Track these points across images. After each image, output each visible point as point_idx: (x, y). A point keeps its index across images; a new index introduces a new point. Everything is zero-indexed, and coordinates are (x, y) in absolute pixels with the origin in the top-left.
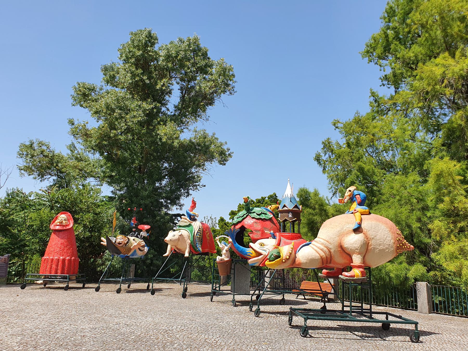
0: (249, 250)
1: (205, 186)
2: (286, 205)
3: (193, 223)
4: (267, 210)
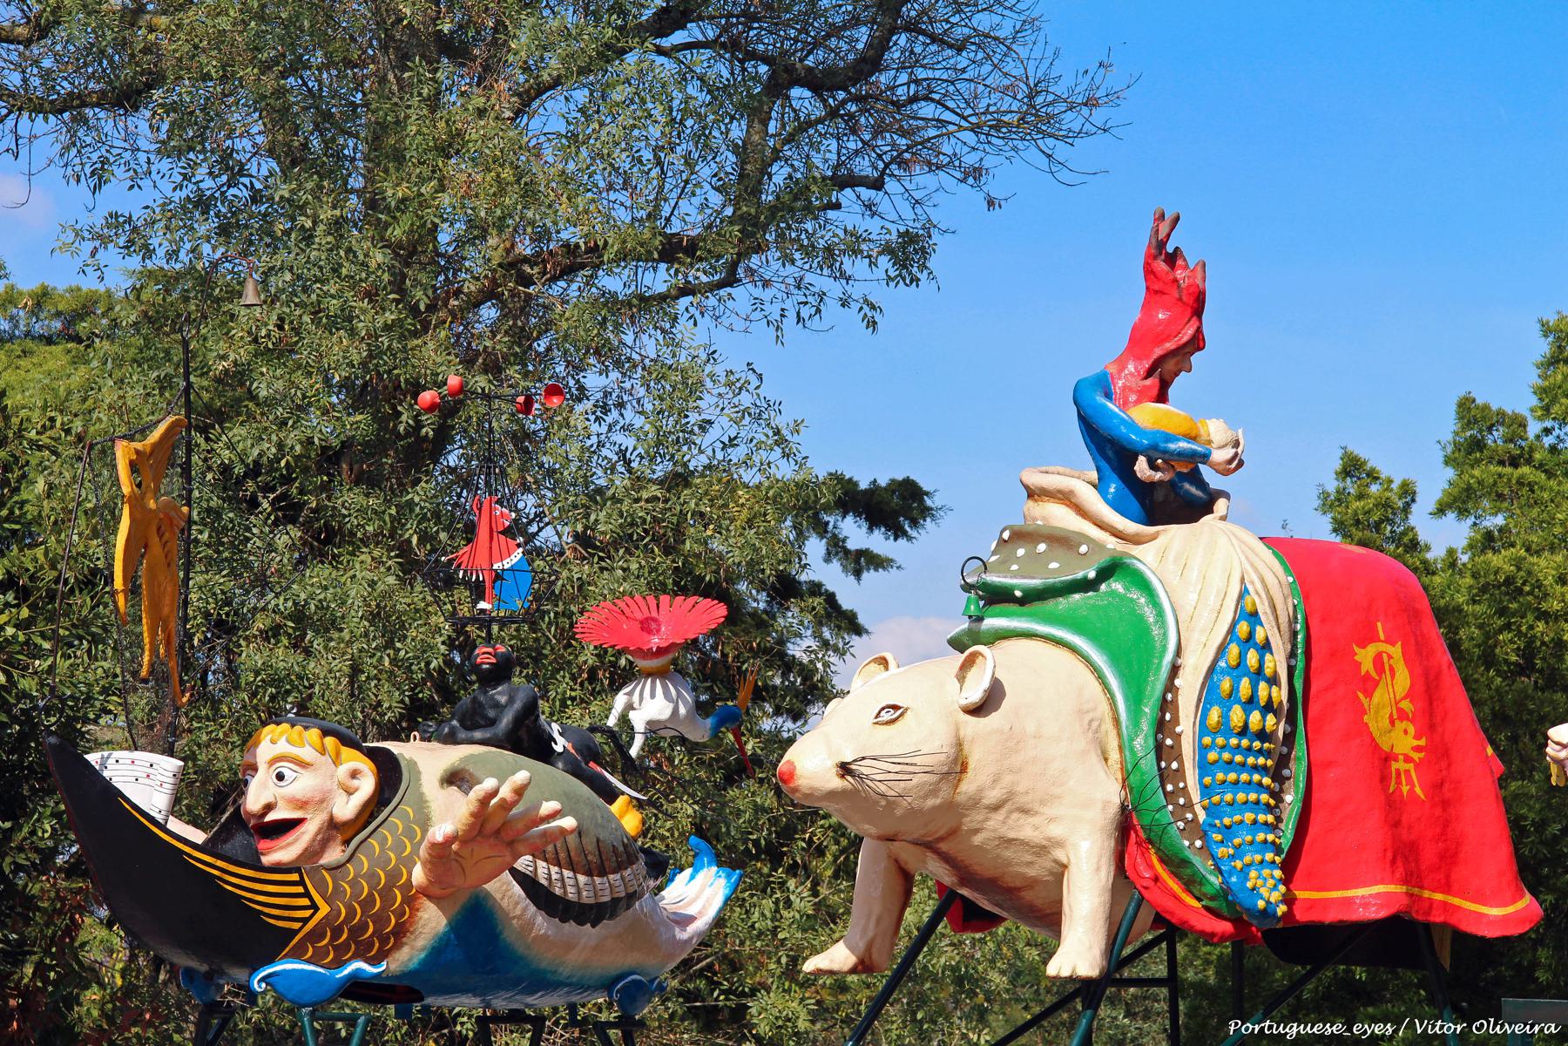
3: (1167, 552)
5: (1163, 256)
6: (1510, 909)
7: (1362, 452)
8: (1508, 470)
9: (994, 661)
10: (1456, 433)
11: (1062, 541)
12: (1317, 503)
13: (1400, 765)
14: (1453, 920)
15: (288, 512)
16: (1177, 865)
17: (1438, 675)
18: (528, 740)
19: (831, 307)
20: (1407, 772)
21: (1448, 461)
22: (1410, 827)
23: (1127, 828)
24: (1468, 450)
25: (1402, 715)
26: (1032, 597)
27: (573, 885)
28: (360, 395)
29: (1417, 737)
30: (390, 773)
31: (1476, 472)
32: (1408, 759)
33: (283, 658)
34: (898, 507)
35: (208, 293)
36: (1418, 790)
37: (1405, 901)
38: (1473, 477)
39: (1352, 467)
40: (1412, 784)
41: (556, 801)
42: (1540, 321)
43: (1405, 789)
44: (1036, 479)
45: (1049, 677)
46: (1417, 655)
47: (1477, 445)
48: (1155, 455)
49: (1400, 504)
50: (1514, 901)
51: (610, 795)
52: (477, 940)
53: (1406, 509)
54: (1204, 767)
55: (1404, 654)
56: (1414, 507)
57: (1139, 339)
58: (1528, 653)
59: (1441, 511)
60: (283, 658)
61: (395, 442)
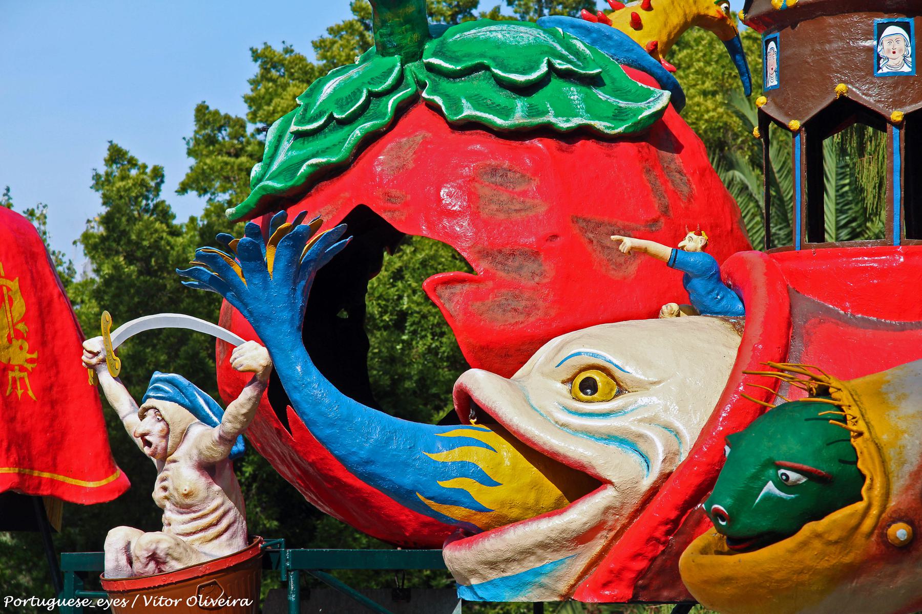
0: (448, 455)
1: (8, 190)
6: (104, 482)
7: (123, 145)
8: (232, 160)
10: (196, 132)
12: (92, 182)
13: (17, 374)
14: (59, 492)
17: (50, 303)
20: (22, 379)
21: (190, 153)
22: (23, 422)
25: (18, 335)
29: (31, 351)
31: (208, 161)
32: (22, 369)
36: (30, 393)
37: (17, 479)
38: (205, 164)
39: (116, 155)
42: (251, 49)
43: (20, 392)
49: (153, 184)
50: (107, 476)
53: (157, 189)
55: (20, 287)
56: (163, 187)
59: (183, 189)
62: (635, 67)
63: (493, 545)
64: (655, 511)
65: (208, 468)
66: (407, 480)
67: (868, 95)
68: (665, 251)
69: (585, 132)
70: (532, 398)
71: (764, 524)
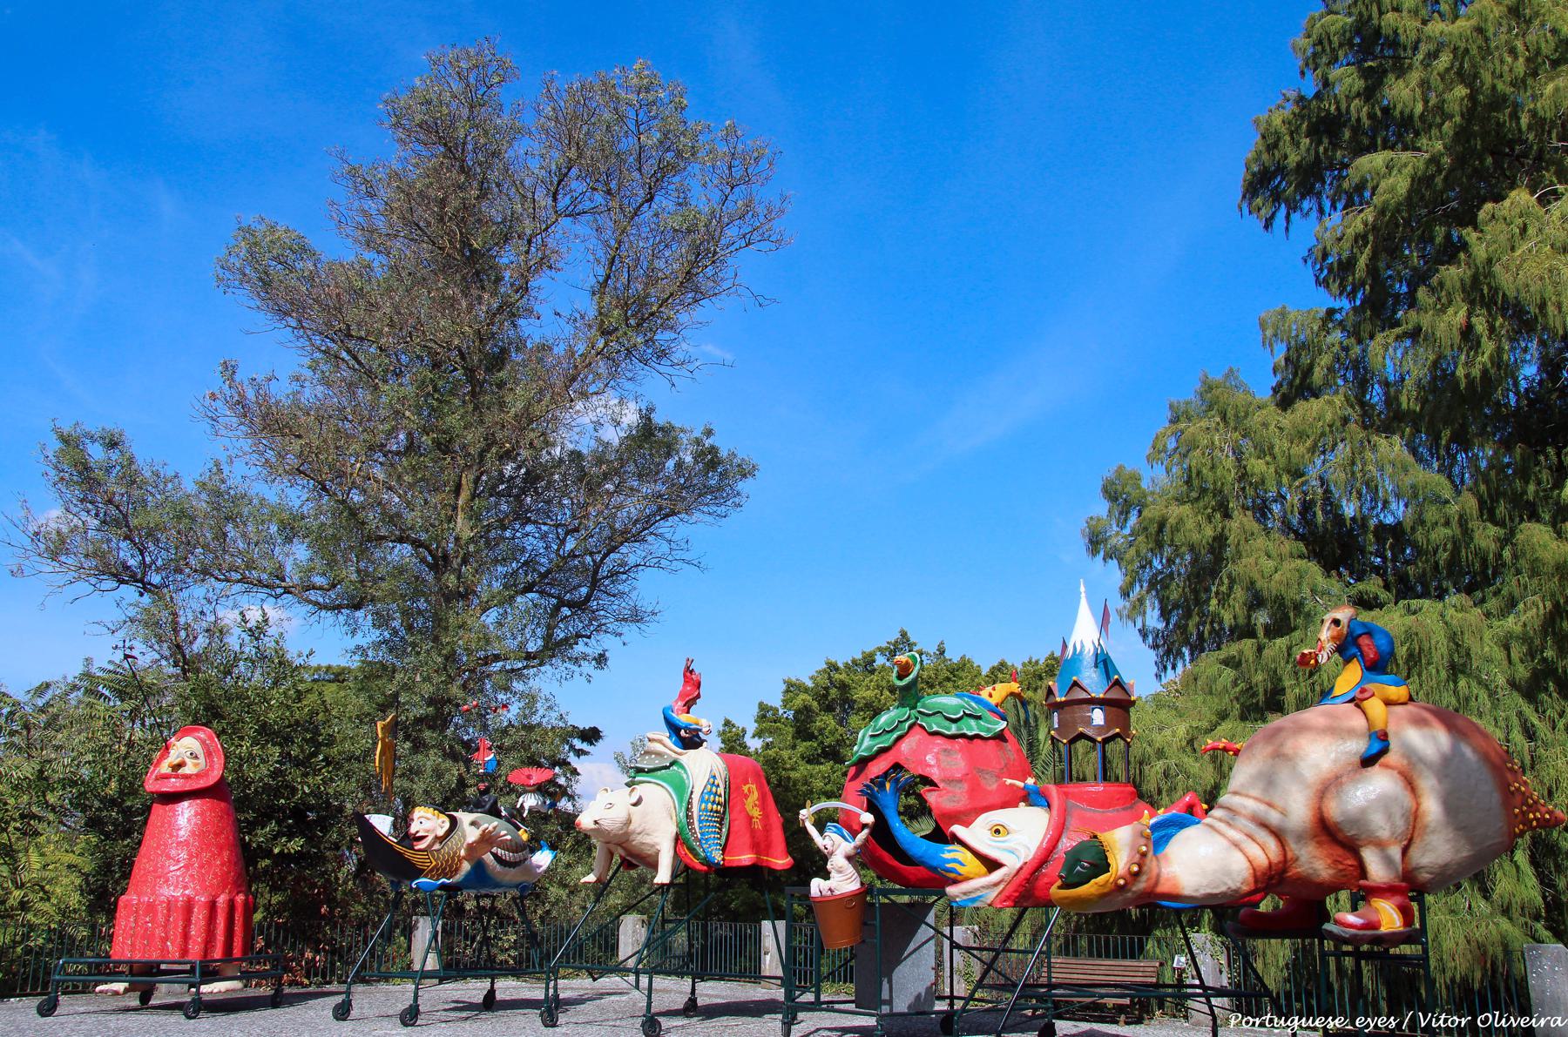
0: (951, 853)
2: (1084, 683)
3: (689, 757)
4: (980, 702)
5: (689, 671)
9: (640, 790)
11: (659, 754)
15: (407, 738)
16: (692, 850)
18: (494, 812)
19: (576, 675)
23: (678, 839)
24: (762, 718)
26: (650, 771)
27: (507, 855)
28: (431, 702)
30: (454, 822)
33: (406, 784)
34: (592, 735)
35: (387, 671)
39: (727, 723)
40: (758, 826)
41: (505, 833)
44: (651, 735)
45: (656, 795)
46: (760, 788)
47: (764, 716)
48: (686, 729)
51: (519, 829)
52: (480, 872)
54: (700, 821)
57: (681, 696)
58: (780, 781)
60: (406, 784)
61: (440, 713)
62: (991, 711)
63: (964, 887)
64: (1023, 875)
65: (849, 858)
66: (934, 863)
67: (1090, 733)
68: (1021, 784)
69: (977, 736)
70: (977, 833)
71: (1076, 880)
